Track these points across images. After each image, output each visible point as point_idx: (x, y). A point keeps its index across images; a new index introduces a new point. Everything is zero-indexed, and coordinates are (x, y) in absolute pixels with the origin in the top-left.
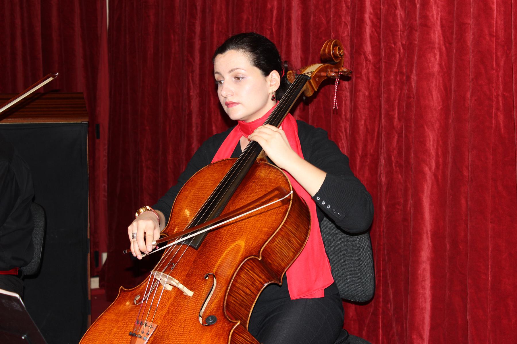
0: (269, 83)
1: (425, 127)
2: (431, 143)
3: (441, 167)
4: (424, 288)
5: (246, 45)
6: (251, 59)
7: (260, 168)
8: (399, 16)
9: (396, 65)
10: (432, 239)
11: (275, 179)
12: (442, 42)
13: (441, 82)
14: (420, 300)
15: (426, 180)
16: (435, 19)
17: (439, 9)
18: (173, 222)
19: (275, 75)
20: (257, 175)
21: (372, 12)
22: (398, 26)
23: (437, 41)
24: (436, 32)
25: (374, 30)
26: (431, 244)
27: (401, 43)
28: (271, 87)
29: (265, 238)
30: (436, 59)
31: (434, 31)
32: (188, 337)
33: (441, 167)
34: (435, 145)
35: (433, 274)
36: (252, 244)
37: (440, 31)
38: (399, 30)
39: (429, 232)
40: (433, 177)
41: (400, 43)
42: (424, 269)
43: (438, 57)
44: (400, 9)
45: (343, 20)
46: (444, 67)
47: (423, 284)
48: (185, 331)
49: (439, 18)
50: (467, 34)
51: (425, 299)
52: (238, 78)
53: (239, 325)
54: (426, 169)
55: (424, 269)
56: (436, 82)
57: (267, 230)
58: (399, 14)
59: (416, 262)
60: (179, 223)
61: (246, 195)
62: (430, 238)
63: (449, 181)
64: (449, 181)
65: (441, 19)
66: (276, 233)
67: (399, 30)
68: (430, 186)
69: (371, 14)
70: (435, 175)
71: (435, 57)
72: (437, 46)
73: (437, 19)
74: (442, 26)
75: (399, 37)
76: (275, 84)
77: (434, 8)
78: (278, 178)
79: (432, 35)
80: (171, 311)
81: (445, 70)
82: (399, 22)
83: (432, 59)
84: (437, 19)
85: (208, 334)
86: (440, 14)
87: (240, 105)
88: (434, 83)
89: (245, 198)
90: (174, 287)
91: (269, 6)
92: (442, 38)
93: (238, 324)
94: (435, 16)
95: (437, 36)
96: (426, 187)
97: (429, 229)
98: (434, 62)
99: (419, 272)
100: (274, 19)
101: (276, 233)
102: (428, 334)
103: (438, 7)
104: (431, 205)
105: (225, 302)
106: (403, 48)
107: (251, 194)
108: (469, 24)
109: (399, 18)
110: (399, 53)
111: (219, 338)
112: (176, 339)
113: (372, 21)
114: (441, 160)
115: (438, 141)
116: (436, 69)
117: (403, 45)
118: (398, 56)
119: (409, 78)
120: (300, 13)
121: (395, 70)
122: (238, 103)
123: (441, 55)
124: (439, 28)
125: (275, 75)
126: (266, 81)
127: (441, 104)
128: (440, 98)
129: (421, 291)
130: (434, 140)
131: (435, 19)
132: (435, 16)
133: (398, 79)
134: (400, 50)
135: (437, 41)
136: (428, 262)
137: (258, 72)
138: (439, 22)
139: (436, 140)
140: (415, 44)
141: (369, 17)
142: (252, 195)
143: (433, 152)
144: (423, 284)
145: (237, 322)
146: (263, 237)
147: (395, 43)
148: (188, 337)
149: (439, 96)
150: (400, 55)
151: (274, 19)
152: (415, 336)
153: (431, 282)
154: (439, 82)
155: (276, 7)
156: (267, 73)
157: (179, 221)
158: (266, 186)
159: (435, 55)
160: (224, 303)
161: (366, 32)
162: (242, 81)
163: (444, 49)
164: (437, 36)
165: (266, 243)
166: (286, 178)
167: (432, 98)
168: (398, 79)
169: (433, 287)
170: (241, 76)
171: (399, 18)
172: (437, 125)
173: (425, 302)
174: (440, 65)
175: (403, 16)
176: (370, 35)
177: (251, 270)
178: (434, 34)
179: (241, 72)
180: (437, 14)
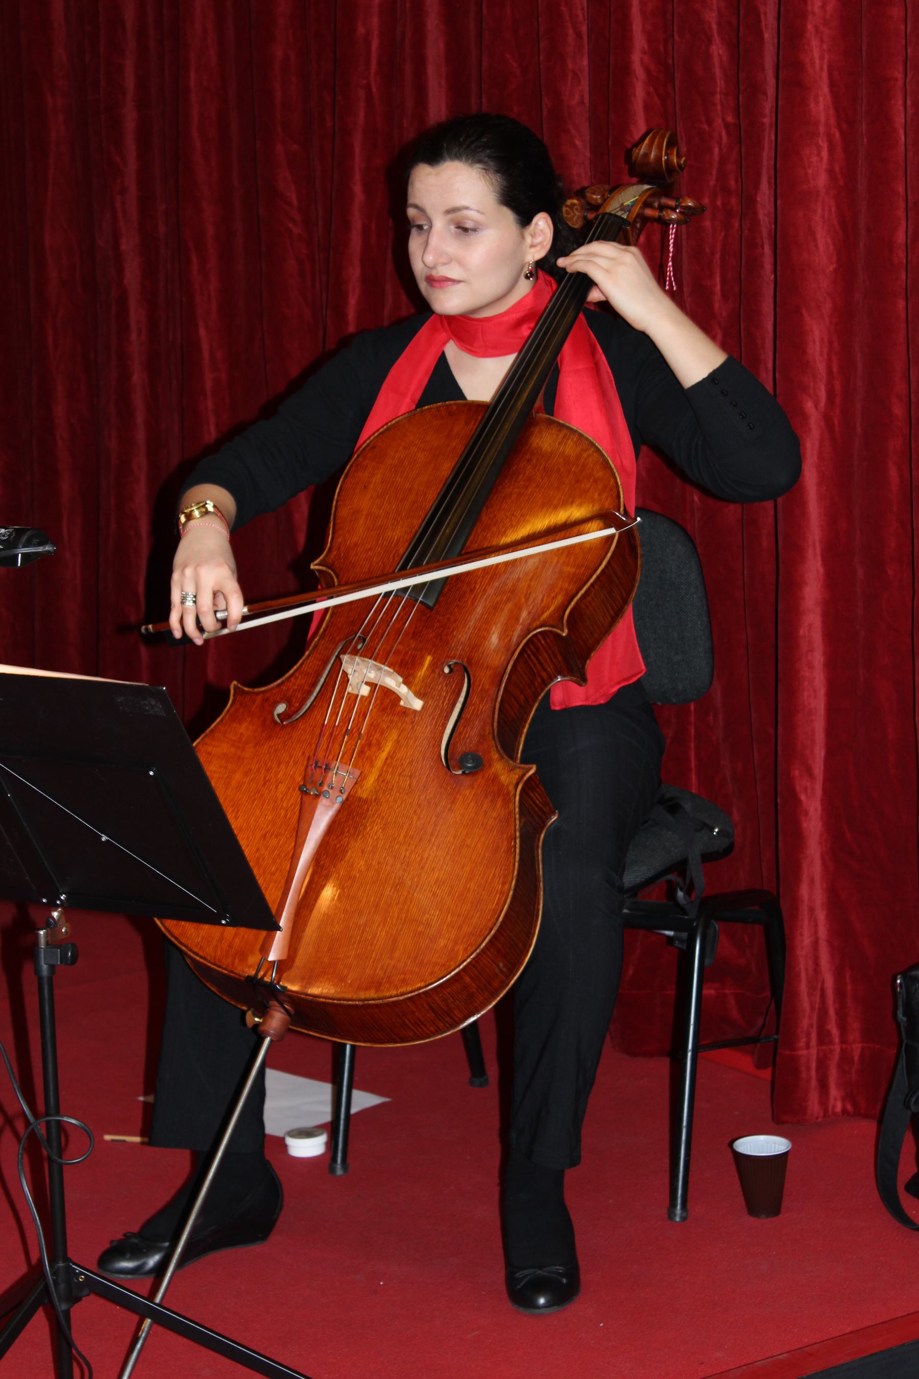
0: (529, 240)
1: (804, 311)
2: (818, 347)
3: (838, 400)
4: (811, 667)
5: (489, 157)
6: (498, 188)
7: (537, 430)
8: (716, 60)
9: (714, 172)
10: (823, 557)
11: (578, 457)
12: (832, 121)
13: (833, 209)
14: (806, 694)
15: (810, 429)
16: (818, 67)
17: (825, 47)
18: (340, 540)
19: (542, 224)
20: (534, 445)
21: (646, 47)
22: (716, 82)
23: (822, 118)
24: (821, 99)
25: (652, 89)
26: (821, 570)
27: (724, 120)
28: (533, 250)
29: (572, 588)
30: (821, 159)
31: (817, 96)
32: (423, 797)
33: (838, 400)
34: (825, 350)
35: (830, 636)
36: (542, 600)
37: (829, 98)
38: (718, 90)
39: (817, 545)
40: (822, 423)
41: (720, 121)
42: (810, 625)
43: (825, 154)
44: (718, 42)
45: (570, 66)
46: (839, 176)
47: (810, 658)
48: (414, 784)
49: (825, 67)
50: (893, 102)
51: (815, 691)
52: (466, 230)
53: (534, 774)
54: (809, 405)
55: (810, 625)
56: (823, 210)
57: (573, 570)
58: (715, 54)
59: (794, 611)
60: (356, 545)
61: (516, 490)
62: (819, 558)
63: (859, 430)
64: (859, 430)
65: (829, 66)
66: (594, 577)
67: (718, 90)
68: (817, 443)
69: (644, 52)
70: (827, 418)
71: (819, 154)
72: (822, 129)
73: (821, 69)
74: (832, 85)
75: (719, 107)
76: (541, 243)
77: (815, 43)
78: (585, 455)
79: (812, 105)
80: (374, 741)
81: (841, 183)
82: (718, 72)
83: (814, 159)
84: (821, 69)
85: (468, 792)
86: (827, 57)
87: (461, 285)
88: (819, 211)
89: (514, 497)
90: (373, 685)
91: (361, 30)
92: (832, 112)
93: (532, 772)
94: (817, 61)
95: (822, 105)
96: (808, 445)
97: (817, 538)
98: (818, 166)
99: (801, 632)
100: (374, 62)
101: (594, 577)
102: (822, 767)
103: (822, 41)
104: (819, 484)
105: (495, 724)
106: (728, 133)
107: (527, 487)
108: (896, 80)
109: (717, 64)
110: (720, 143)
111: (492, 801)
112: (395, 802)
113: (647, 71)
114: (837, 384)
115: (830, 343)
116: (822, 181)
117: (727, 125)
118: (716, 150)
119: (749, 203)
120: (442, 45)
121: (712, 183)
122: (459, 282)
123: (831, 150)
124: (825, 89)
125: (542, 224)
126: (523, 237)
127: (834, 259)
128: (831, 247)
129: (805, 673)
130: (822, 340)
131: (818, 67)
132: (817, 61)
133: (719, 203)
134: (720, 136)
135: (822, 118)
136: (818, 610)
137: (508, 216)
138: (825, 75)
139: (826, 339)
140: (763, 124)
141: (642, 60)
142: (530, 490)
143: (821, 367)
144: (810, 658)
145: (531, 769)
146: (566, 585)
147: (710, 123)
148: (423, 797)
149: (829, 240)
150: (720, 149)
151: (374, 62)
152: (797, 773)
153: (825, 654)
154: (830, 211)
155: (376, 33)
156: (525, 220)
157: (355, 539)
158: (558, 470)
159: (819, 148)
160: (493, 725)
161: (635, 95)
162: (473, 237)
163: (838, 135)
164: (822, 105)
165: (576, 600)
166: (603, 456)
167: (816, 246)
168: (719, 203)
169: (831, 664)
170: (469, 225)
171: (717, 64)
172: (827, 307)
173: (815, 697)
174: (831, 172)
175: (725, 58)
176: (644, 102)
177: (535, 656)
178: (817, 102)
179: (472, 216)
180: (822, 58)
